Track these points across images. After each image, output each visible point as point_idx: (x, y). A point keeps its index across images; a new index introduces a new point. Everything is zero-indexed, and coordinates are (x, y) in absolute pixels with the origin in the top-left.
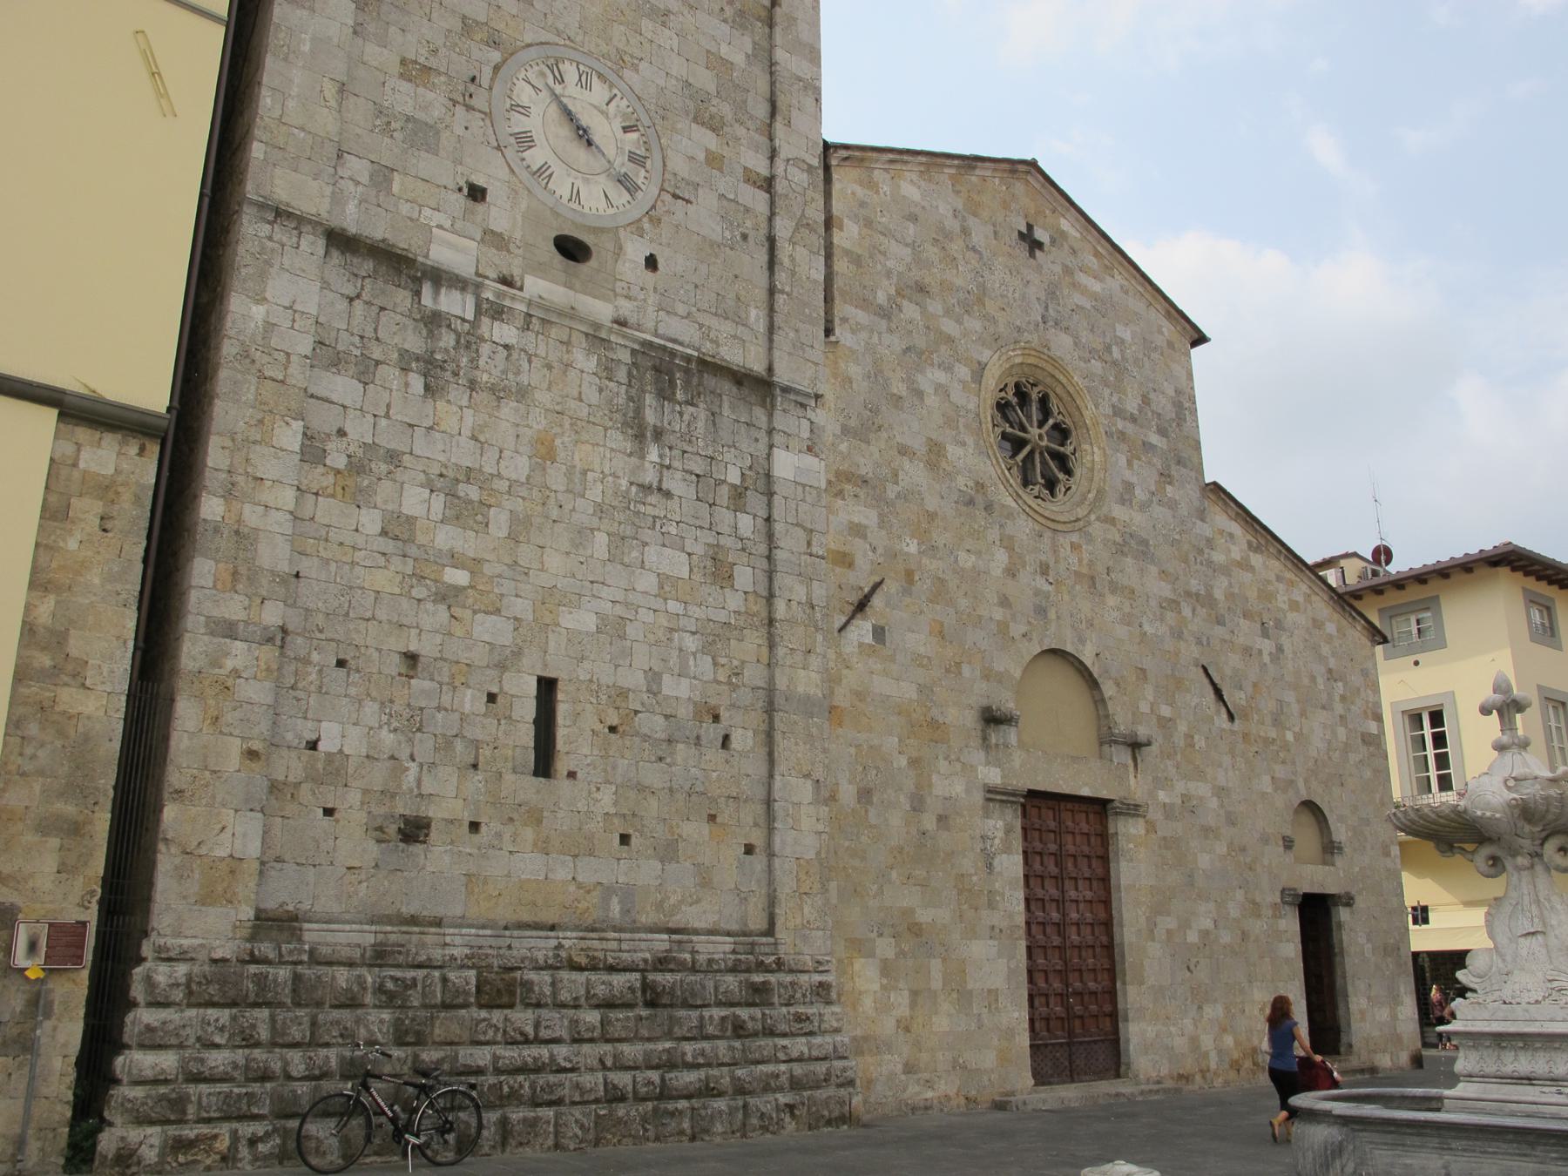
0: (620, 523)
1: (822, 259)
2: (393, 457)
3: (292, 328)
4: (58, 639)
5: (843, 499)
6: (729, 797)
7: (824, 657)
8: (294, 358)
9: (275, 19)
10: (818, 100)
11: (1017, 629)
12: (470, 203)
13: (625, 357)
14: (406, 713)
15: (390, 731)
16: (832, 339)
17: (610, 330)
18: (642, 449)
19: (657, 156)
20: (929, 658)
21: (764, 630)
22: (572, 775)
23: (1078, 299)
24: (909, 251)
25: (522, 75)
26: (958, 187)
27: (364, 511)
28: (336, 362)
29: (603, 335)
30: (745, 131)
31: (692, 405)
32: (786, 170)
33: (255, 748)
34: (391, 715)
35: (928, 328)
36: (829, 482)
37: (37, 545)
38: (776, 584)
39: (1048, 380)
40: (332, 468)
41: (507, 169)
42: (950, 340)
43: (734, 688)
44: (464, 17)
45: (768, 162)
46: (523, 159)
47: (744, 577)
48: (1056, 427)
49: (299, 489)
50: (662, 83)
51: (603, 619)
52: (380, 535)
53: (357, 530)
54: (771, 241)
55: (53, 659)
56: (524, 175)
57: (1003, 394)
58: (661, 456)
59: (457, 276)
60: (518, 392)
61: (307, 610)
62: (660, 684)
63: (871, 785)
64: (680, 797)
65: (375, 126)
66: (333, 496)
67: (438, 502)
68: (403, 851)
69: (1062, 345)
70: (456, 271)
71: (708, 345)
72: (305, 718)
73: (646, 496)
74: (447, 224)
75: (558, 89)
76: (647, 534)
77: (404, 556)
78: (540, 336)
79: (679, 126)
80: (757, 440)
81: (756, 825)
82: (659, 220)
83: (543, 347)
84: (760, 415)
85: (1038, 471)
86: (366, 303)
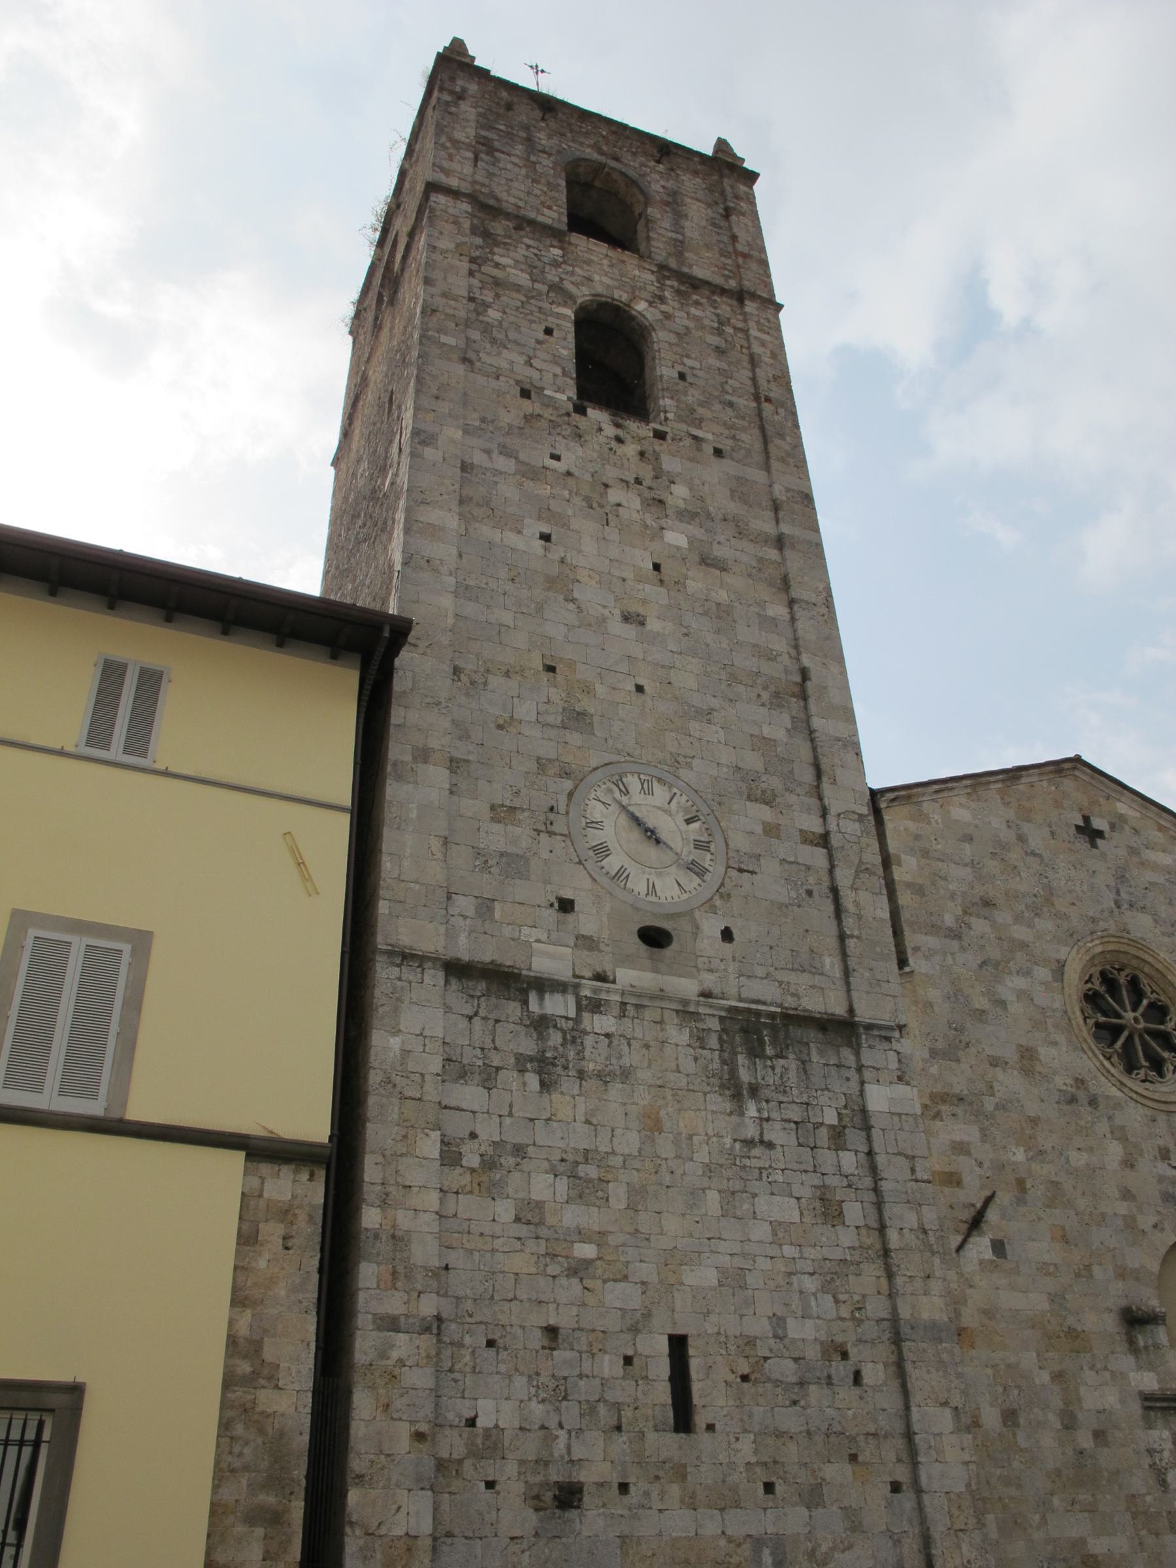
0: (729, 1179)
1: (885, 899)
2: (519, 1150)
3: (424, 1051)
4: (256, 1347)
5: (942, 1120)
6: (867, 1434)
7: (945, 1280)
8: (427, 1077)
9: (388, 797)
10: (858, 754)
11: (1146, 1221)
12: (561, 915)
13: (715, 1024)
14: (552, 1384)
15: (539, 1402)
16: (907, 969)
17: (698, 1003)
18: (740, 1107)
19: (719, 837)
20: (1055, 1265)
21: (880, 1262)
22: (710, 1428)
23: (1149, 876)
24: (969, 870)
25: (592, 796)
26: (1007, 799)
27: (498, 1202)
28: (463, 1074)
29: (692, 1009)
30: (796, 797)
31: (783, 1057)
32: (838, 825)
33: (421, 1430)
34: (538, 1387)
35: (1000, 939)
36: (925, 1107)
37: (236, 1268)
38: (886, 1214)
39: (1134, 962)
40: (468, 1168)
41: (589, 880)
42: (1024, 945)
43: (859, 1322)
44: (538, 759)
45: (821, 820)
46: (603, 868)
47: (854, 1212)
48: (1152, 1005)
49: (441, 1190)
50: (714, 773)
51: (723, 1273)
52: (515, 1221)
53: (494, 1220)
54: (835, 891)
55: (252, 1366)
56: (605, 881)
57: (1089, 985)
58: (759, 1111)
59: (557, 981)
60: (622, 1074)
61: (457, 1298)
62: (785, 1328)
63: (1015, 1406)
64: (819, 1438)
65: (475, 867)
66: (471, 1192)
67: (562, 1185)
68: (559, 1518)
69: (1141, 925)
70: (556, 977)
71: (789, 999)
72: (463, 1398)
73: (749, 1150)
74: (544, 937)
75: (625, 800)
76: (755, 1187)
77: (537, 1238)
78: (635, 1020)
79: (735, 807)
80: (848, 1079)
81: (899, 1460)
82: (729, 895)
83: (640, 1030)
84: (848, 1056)
85: (1141, 1054)
86: (484, 1018)
